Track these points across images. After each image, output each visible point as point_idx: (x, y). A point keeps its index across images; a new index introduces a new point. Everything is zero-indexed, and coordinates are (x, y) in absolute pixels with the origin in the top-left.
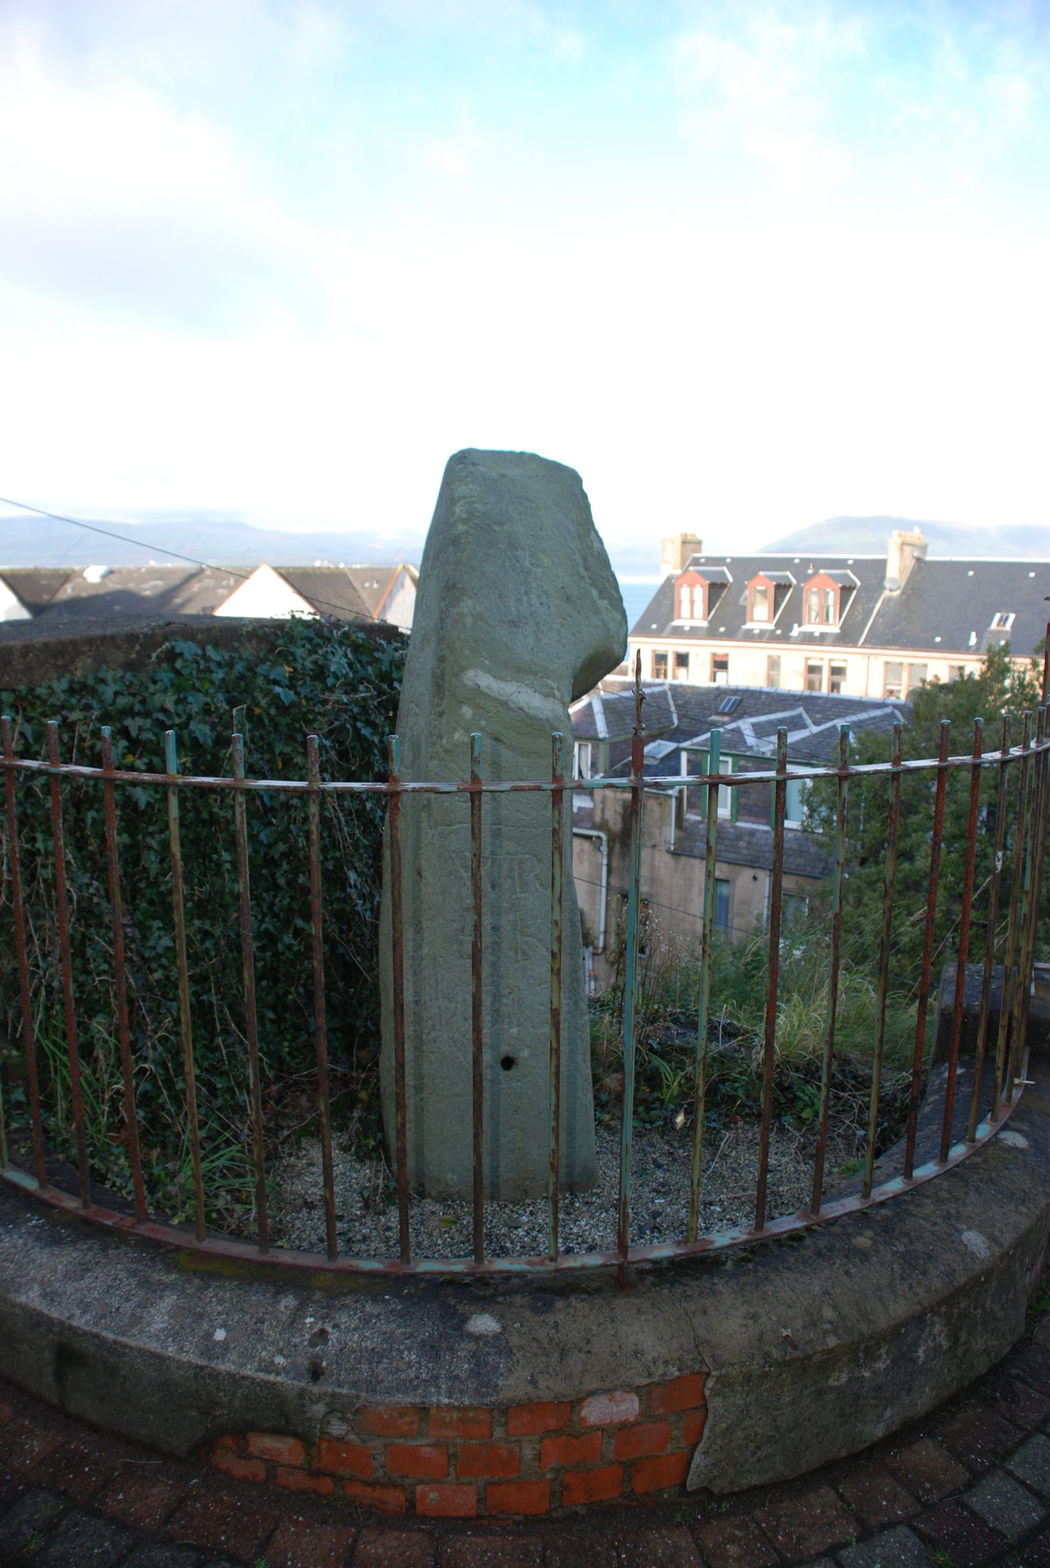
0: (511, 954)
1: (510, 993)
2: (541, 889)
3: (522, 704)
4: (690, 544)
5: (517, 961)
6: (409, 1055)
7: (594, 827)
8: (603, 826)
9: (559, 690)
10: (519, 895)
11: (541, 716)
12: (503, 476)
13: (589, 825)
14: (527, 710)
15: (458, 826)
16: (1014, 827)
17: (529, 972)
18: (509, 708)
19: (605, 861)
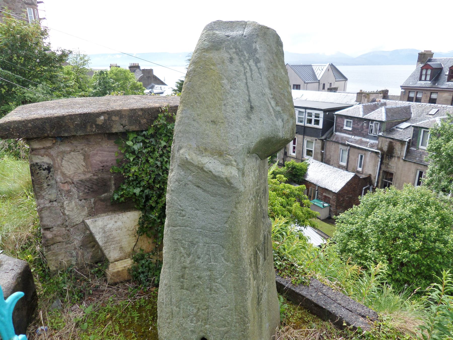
0: (208, 290)
1: (206, 309)
2: (225, 262)
3: (212, 169)
4: (425, 58)
5: (210, 294)
6: (266, 251)
7: (378, 149)
8: (381, 149)
9: (235, 161)
10: (212, 263)
11: (223, 176)
12: (228, 36)
13: (376, 148)
14: (214, 173)
15: (179, 228)
16: (403, 321)
17: (216, 300)
18: (204, 171)
19: (380, 160)
